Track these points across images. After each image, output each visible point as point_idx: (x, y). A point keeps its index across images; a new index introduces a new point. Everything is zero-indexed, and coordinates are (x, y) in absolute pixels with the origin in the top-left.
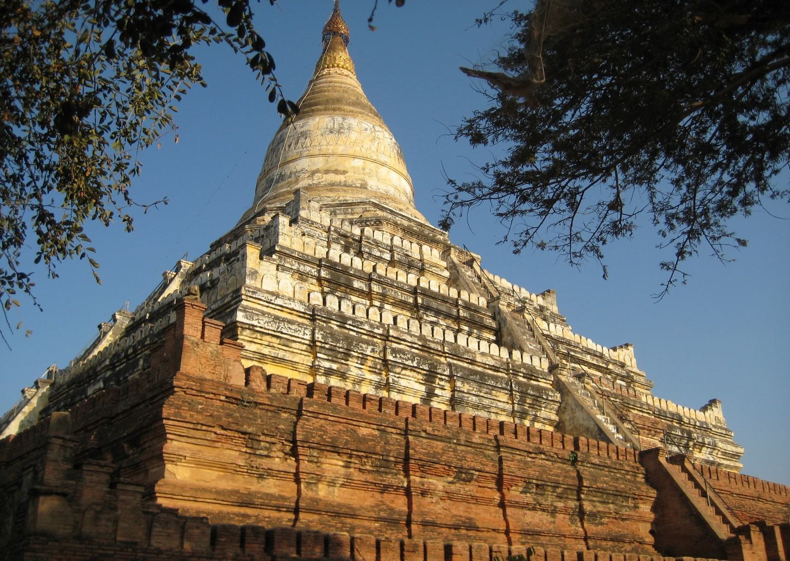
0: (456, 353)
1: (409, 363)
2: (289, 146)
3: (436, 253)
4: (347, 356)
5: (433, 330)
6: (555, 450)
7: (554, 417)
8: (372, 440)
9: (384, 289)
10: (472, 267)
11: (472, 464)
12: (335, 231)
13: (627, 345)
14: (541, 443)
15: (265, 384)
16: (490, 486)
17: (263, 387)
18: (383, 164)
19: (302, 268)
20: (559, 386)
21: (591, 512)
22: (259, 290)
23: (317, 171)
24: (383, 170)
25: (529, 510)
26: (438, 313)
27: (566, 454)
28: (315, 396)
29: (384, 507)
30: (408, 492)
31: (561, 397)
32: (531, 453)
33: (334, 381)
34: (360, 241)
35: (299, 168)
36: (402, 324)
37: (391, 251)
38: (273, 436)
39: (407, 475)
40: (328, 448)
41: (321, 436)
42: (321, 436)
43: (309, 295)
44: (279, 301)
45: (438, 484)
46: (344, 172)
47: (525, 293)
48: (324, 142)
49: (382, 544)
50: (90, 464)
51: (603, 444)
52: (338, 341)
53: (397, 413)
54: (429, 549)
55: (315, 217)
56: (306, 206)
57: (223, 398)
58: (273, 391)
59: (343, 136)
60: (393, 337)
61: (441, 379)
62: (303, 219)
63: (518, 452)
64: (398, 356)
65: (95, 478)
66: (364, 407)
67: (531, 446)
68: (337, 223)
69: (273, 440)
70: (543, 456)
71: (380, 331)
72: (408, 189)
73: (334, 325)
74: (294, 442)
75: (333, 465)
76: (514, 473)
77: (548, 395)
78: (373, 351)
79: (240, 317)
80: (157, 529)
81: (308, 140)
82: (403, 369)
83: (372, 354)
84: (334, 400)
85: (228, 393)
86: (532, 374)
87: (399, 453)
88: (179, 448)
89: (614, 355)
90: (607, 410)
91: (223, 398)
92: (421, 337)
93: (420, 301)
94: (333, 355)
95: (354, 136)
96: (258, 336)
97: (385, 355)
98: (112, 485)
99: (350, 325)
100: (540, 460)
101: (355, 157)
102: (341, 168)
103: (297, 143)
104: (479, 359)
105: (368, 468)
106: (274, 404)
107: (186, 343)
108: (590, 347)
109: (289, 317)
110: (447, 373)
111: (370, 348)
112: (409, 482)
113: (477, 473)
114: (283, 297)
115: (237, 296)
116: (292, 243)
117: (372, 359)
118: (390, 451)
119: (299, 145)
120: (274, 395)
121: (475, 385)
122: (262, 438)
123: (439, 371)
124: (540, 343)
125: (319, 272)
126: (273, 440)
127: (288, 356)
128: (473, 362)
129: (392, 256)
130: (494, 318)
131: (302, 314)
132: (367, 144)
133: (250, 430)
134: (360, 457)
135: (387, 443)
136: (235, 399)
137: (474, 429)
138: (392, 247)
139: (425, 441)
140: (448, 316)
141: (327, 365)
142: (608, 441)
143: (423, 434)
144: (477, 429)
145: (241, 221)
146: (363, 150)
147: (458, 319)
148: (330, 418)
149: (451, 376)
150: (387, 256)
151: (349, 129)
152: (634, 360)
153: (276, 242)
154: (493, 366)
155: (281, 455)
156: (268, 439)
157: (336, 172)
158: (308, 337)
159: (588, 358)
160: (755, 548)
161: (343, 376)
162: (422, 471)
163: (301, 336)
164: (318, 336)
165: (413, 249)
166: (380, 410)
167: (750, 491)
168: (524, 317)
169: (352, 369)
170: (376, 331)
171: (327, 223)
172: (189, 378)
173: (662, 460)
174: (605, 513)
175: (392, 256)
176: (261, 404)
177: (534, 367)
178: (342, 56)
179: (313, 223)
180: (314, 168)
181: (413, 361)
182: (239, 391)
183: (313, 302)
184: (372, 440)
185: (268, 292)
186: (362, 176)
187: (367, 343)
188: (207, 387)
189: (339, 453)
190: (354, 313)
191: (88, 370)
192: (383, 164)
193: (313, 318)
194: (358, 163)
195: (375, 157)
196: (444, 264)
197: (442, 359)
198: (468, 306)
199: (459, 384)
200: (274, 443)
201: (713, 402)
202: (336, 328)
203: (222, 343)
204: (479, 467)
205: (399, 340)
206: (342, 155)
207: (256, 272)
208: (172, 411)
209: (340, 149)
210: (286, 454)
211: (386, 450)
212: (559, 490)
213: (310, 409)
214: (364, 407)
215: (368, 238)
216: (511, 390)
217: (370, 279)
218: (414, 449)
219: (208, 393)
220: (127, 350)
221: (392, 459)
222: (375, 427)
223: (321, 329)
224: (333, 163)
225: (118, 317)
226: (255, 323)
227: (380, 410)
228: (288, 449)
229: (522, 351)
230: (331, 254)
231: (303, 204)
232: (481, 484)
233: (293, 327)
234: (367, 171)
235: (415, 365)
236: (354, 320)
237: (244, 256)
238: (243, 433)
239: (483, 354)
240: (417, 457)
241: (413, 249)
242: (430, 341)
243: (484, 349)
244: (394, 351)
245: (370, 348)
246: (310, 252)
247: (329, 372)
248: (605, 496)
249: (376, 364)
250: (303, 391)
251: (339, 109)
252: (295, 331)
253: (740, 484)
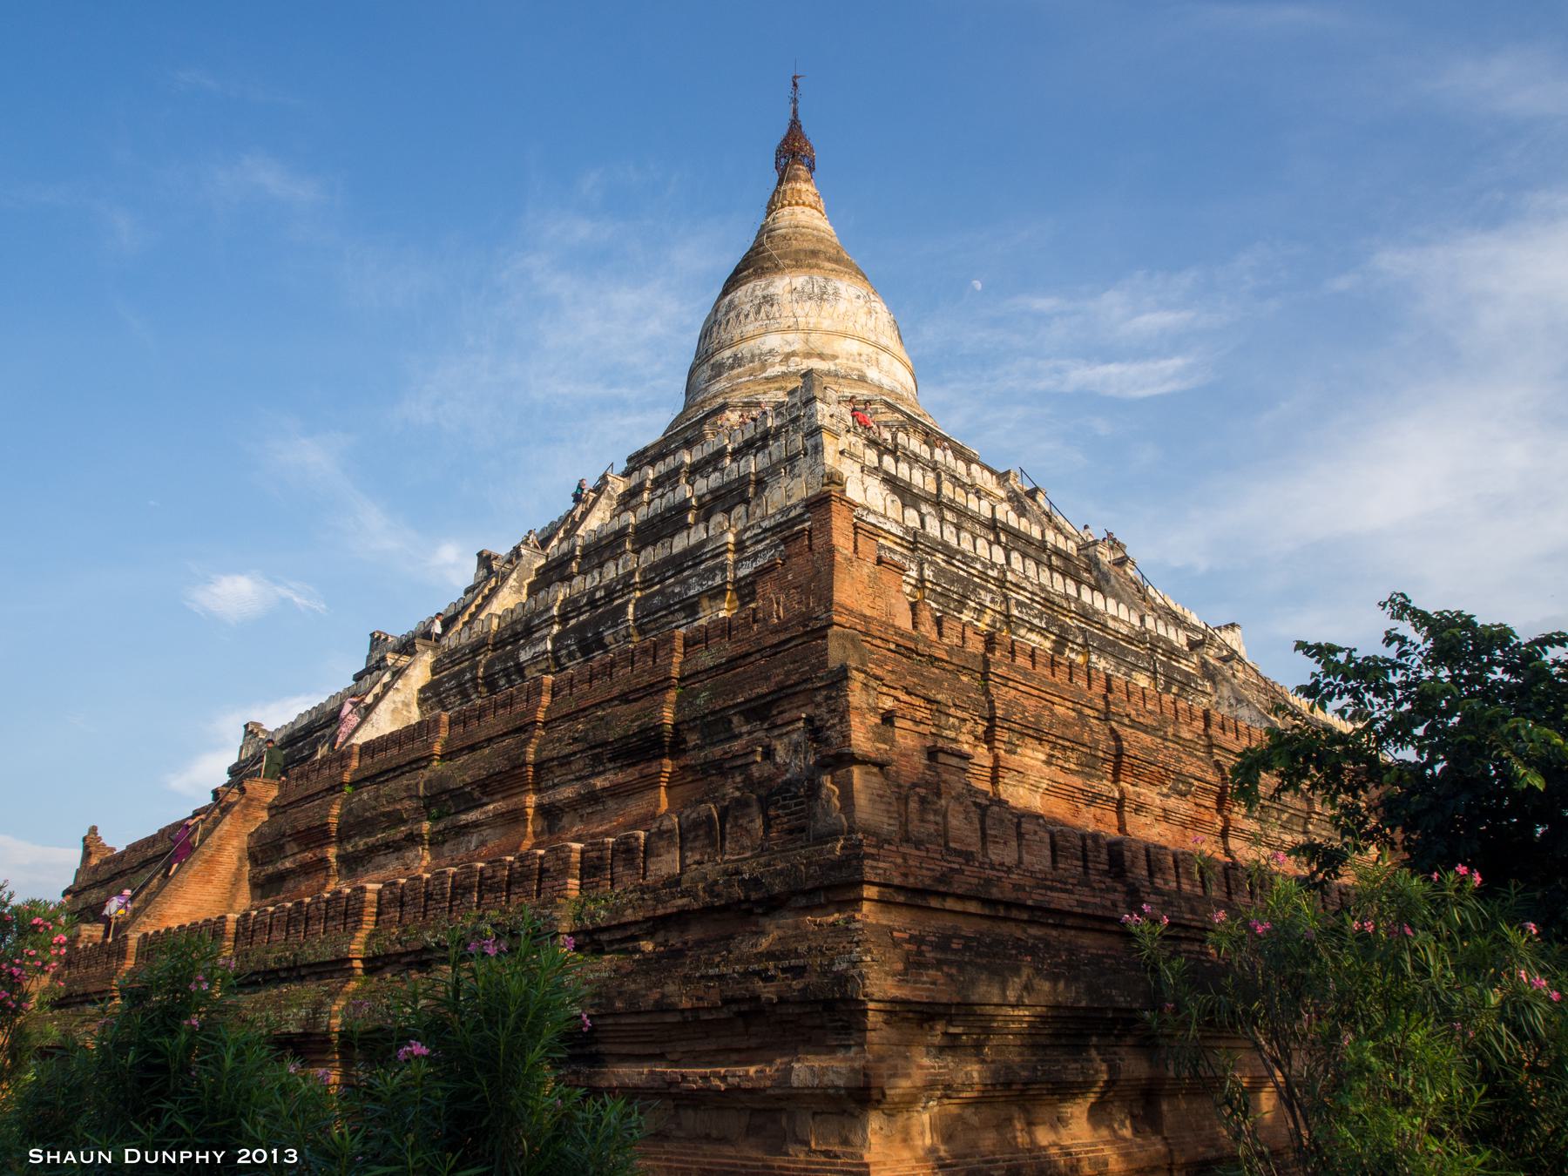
0: (1086, 614)
1: (1036, 621)
2: (747, 316)
16: (1207, 804)
18: (885, 350)
23: (793, 354)
24: (884, 357)
30: (1120, 805)
35: (765, 348)
38: (964, 709)
39: (1116, 781)
40: (1031, 732)
45: (1151, 795)
46: (834, 357)
48: (799, 312)
57: (892, 646)
59: (826, 306)
61: (1072, 650)
69: (965, 715)
74: (991, 719)
75: (1032, 756)
81: (775, 308)
82: (1030, 630)
85: (901, 641)
91: (892, 646)
92: (1042, 588)
95: (842, 306)
101: (845, 335)
102: (827, 351)
103: (758, 312)
104: (1111, 623)
105: (1073, 766)
106: (955, 660)
107: (838, 558)
112: (1121, 791)
114: (875, 513)
119: (763, 314)
121: (1113, 662)
122: (952, 711)
126: (965, 715)
128: (1104, 627)
132: (862, 318)
133: (939, 697)
134: (1064, 748)
136: (907, 648)
143: (1126, 721)
145: (671, 427)
148: (1021, 688)
149: (1085, 645)
151: (836, 293)
155: (971, 739)
156: (959, 713)
157: (821, 356)
162: (1135, 776)
176: (937, 659)
178: (806, 188)
180: (788, 349)
186: (857, 365)
188: (874, 629)
189: (1040, 740)
191: (514, 622)
192: (885, 350)
194: (853, 346)
195: (873, 338)
199: (1094, 658)
200: (964, 720)
204: (1198, 774)
206: (828, 333)
209: (826, 324)
210: (976, 738)
212: (1285, 816)
213: (999, 671)
216: (1155, 672)
219: (874, 637)
220: (593, 593)
221: (1101, 754)
222: (1069, 704)
224: (816, 341)
225: (523, 552)
228: (980, 729)
238: (929, 701)
240: (1131, 753)
244: (1019, 604)
249: (994, 621)
251: (817, 266)
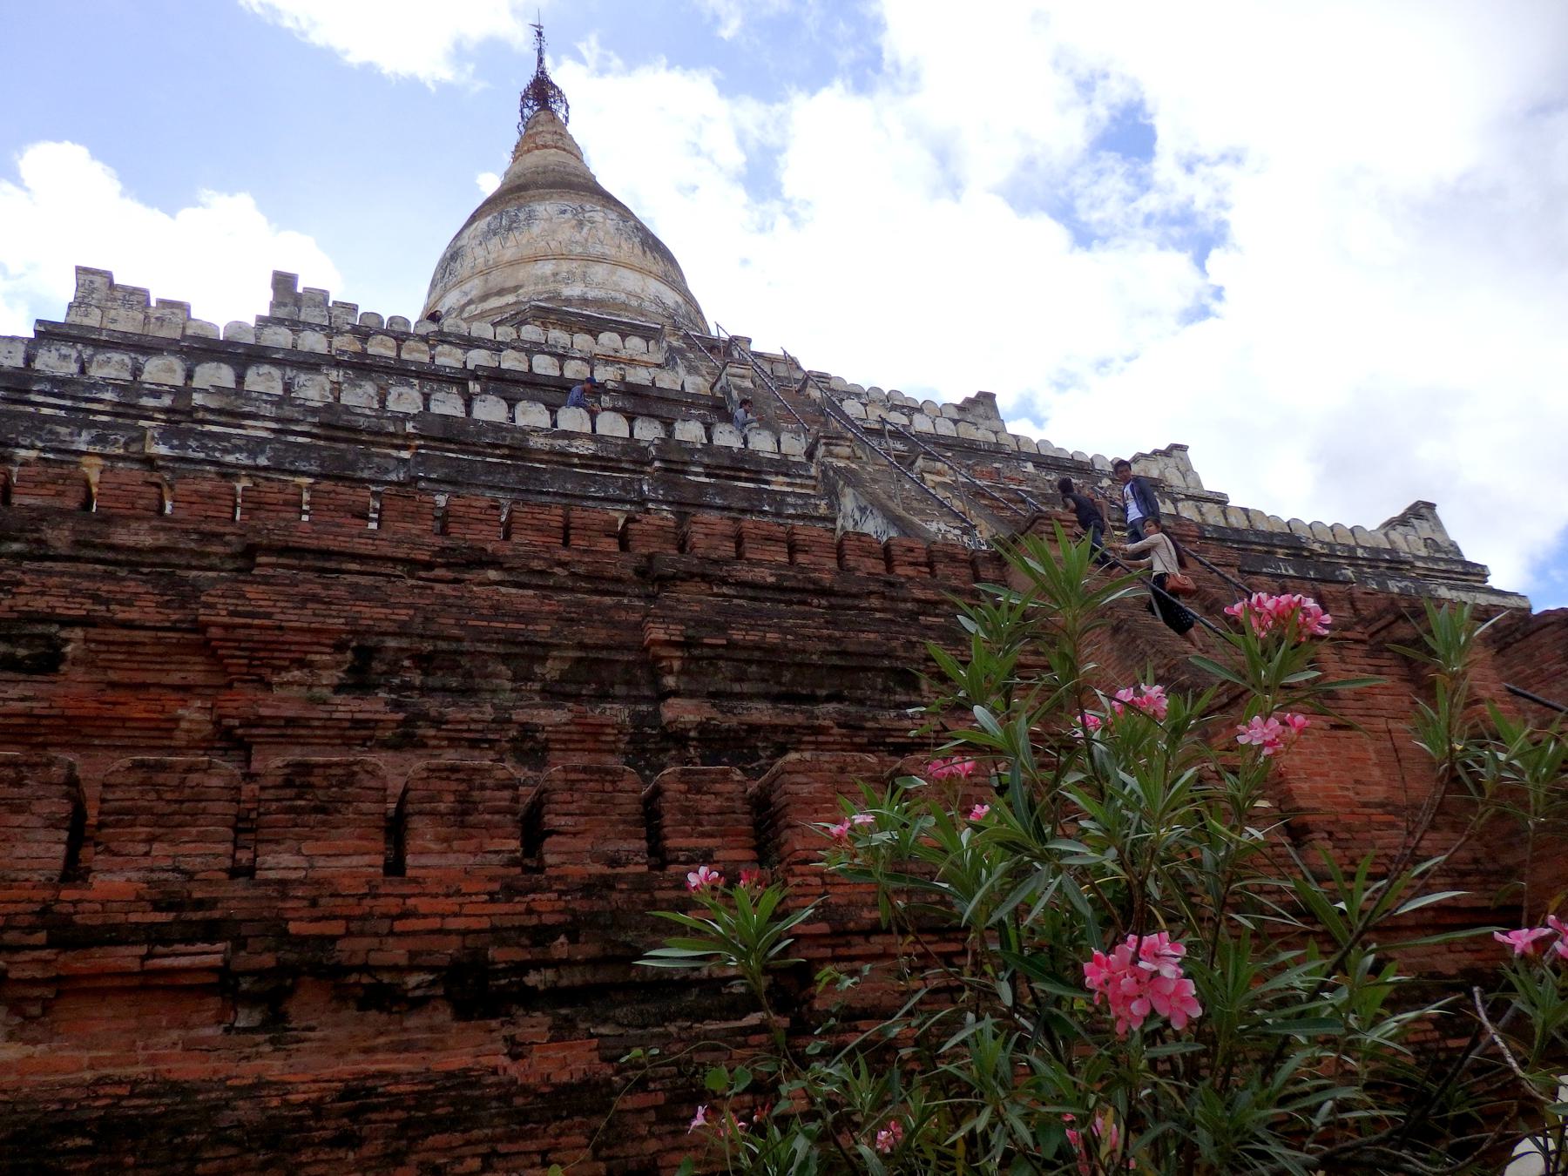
11: (40, 604)
21: (702, 727)
25: (385, 745)
32: (429, 566)
60: (206, 409)
63: (354, 567)
64: (194, 444)
70: (492, 574)
76: (268, 616)
83: (98, 449)
95: (536, 229)
99: (40, 392)
113: (78, 633)
117: (99, 461)
146: (553, 244)
154: (594, 457)
157: (501, 292)
174: (789, 730)
177: (754, 453)
181: (253, 454)
232: (113, 676)
235: (262, 461)
248: (787, 676)
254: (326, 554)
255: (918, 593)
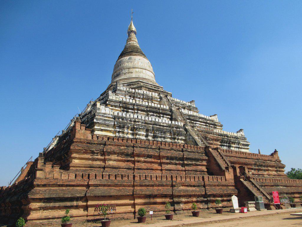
3: (156, 94)
4: (124, 127)
5: (148, 118)
6: (177, 148)
7: (184, 138)
8: (124, 150)
9: (138, 107)
10: (167, 97)
12: (127, 92)
13: (215, 115)
14: (173, 147)
15: (97, 138)
17: (96, 139)
19: (115, 104)
20: (186, 130)
22: (100, 113)
26: (153, 112)
27: (181, 149)
28: (110, 140)
29: (128, 165)
31: (186, 133)
33: (121, 135)
34: (134, 94)
36: (139, 117)
37: (143, 95)
41: (110, 150)
42: (110, 150)
43: (114, 113)
44: (105, 115)
47: (184, 102)
49: (117, 175)
50: (47, 163)
51: (196, 146)
52: (121, 124)
53: (132, 142)
54: (129, 176)
55: (122, 88)
56: (119, 86)
58: (99, 140)
62: (118, 89)
65: (49, 166)
66: (123, 142)
67: (169, 148)
68: (128, 89)
71: (133, 120)
72: (153, 75)
73: (120, 120)
77: (182, 132)
78: (131, 125)
79: (95, 120)
80: (63, 175)
84: (115, 140)
86: (178, 127)
87: (131, 152)
88: (75, 155)
89: (210, 118)
90: (199, 135)
93: (148, 109)
94: (120, 127)
96: (100, 125)
97: (134, 126)
98: (52, 167)
100: (172, 151)
107: (77, 131)
108: (202, 117)
109: (108, 119)
110: (152, 129)
111: (130, 125)
115: (94, 115)
116: (113, 98)
118: (129, 152)
120: (99, 141)
123: (150, 129)
124: (183, 118)
125: (120, 105)
127: (108, 129)
129: (143, 97)
130: (170, 112)
131: (112, 118)
135: (128, 150)
137: (153, 144)
138: (143, 94)
139: (139, 148)
140: (156, 113)
141: (118, 130)
142: (197, 145)
143: (139, 147)
144: (154, 144)
147: (159, 113)
150: (142, 97)
152: (217, 119)
153: (109, 98)
158: (113, 124)
159: (200, 120)
160: (230, 173)
161: (123, 133)
163: (111, 123)
164: (116, 123)
165: (150, 94)
166: (127, 142)
167: (243, 156)
168: (179, 111)
169: (125, 130)
170: (132, 120)
171: (125, 90)
172: (77, 139)
173: (210, 149)
175: (143, 97)
179: (121, 90)
182: (90, 141)
183: (115, 114)
184: (124, 150)
185: (103, 113)
187: (129, 123)
189: (115, 154)
190: (126, 116)
193: (114, 119)
196: (159, 97)
197: (151, 126)
198: (163, 110)
201: (241, 130)
202: (121, 120)
203: (85, 130)
205: (138, 122)
207: (99, 108)
208: (73, 147)
211: (127, 152)
214: (123, 142)
215: (136, 92)
216: (171, 132)
217: (134, 105)
218: (135, 151)
223: (116, 121)
226: (99, 122)
227: (127, 142)
229: (177, 121)
230: (123, 100)
231: (118, 85)
233: (109, 122)
234: (140, 71)
236: (126, 118)
237: (96, 104)
239: (164, 123)
240: (136, 153)
241: (150, 94)
242: (147, 121)
243: (165, 121)
245: (130, 125)
246: (117, 99)
247: (119, 132)
250: (107, 139)
252: (110, 122)
253: (240, 154)
254: (163, 149)
255: (199, 152)
